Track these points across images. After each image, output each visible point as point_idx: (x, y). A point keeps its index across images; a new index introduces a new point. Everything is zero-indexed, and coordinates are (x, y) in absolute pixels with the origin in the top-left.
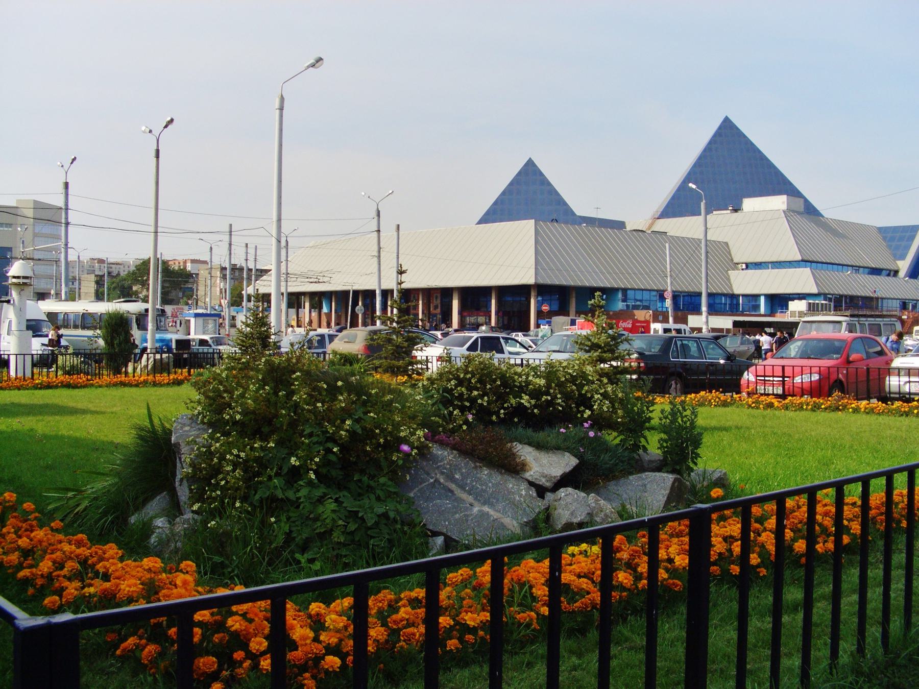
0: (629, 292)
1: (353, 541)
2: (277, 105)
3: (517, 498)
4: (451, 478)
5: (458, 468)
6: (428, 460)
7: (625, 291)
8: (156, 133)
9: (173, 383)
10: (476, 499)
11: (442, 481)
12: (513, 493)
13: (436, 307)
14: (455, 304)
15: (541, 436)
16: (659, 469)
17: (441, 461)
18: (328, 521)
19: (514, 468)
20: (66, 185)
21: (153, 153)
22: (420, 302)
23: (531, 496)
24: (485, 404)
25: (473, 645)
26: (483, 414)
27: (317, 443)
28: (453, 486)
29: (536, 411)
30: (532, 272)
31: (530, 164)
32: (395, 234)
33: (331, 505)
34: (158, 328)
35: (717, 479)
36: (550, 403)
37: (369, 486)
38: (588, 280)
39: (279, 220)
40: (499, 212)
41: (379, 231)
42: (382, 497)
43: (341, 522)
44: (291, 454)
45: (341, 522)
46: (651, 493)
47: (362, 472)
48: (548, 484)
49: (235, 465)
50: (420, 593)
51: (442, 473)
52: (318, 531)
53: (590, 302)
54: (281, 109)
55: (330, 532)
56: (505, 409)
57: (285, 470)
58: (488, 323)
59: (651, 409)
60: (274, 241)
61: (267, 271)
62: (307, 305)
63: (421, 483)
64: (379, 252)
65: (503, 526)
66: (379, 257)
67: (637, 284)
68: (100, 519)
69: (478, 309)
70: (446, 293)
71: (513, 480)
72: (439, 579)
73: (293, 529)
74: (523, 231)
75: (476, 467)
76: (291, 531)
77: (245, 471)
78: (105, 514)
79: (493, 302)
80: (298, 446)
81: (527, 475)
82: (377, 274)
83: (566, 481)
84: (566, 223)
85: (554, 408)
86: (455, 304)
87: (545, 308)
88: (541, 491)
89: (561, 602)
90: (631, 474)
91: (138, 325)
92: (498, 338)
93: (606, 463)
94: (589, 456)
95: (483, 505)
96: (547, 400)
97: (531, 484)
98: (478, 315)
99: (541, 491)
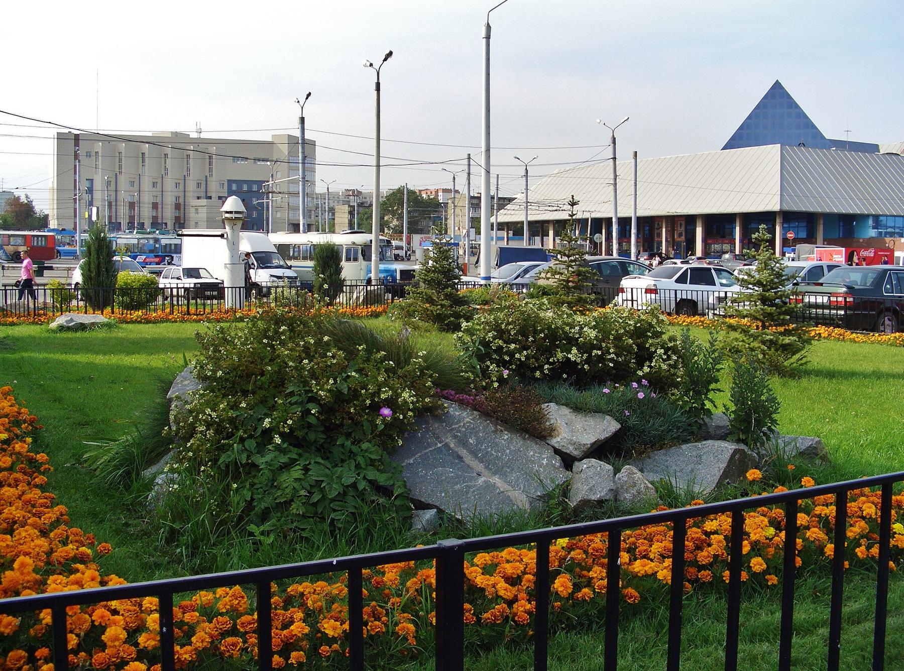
0: (881, 218)
1: (316, 513)
2: (484, 34)
3: (536, 468)
4: (464, 443)
5: (474, 431)
6: (442, 421)
7: (876, 217)
8: (376, 66)
9: (371, 316)
10: (487, 467)
11: (452, 445)
12: (533, 462)
13: (680, 235)
14: (699, 231)
15: (588, 397)
16: (723, 438)
17: (457, 423)
18: (287, 491)
19: (537, 431)
20: (302, 120)
21: (374, 87)
22: (664, 230)
23: (554, 466)
24: (523, 359)
25: (328, 658)
26: (524, 371)
27: (296, 403)
28: (463, 452)
29: (586, 367)
30: (778, 198)
31: (777, 86)
32: (633, 161)
33: (297, 472)
34: (382, 258)
35: (807, 449)
36: (601, 359)
37: (351, 452)
38: (835, 206)
39: (488, 150)
40: (743, 138)
41: (614, 158)
42: (363, 464)
43: (303, 493)
44: (267, 415)
45: (303, 493)
46: (701, 467)
47: (348, 435)
48: (576, 453)
49: (209, 425)
50: (831, 511)
51: (455, 437)
52: (277, 501)
53: (753, 236)
54: (488, 37)
55: (289, 503)
56: (550, 364)
57: (259, 431)
58: (732, 251)
59: (718, 367)
60: (483, 172)
61: (510, 200)
62: (551, 233)
63: (426, 448)
64: (615, 179)
65: (509, 501)
66: (616, 184)
67: (881, 209)
68: (111, 472)
69: (723, 237)
70: (690, 220)
71: (535, 447)
72: (423, 559)
73: (255, 497)
74: (767, 157)
75: (495, 431)
76: (252, 499)
77: (217, 432)
78: (117, 468)
79: (738, 229)
80: (273, 408)
81: (554, 442)
82: (613, 203)
83: (599, 450)
84: (815, 146)
85: (604, 364)
86: (699, 231)
87: (790, 235)
88: (568, 461)
89: (462, 611)
90: (686, 441)
91: (363, 255)
92: (710, 269)
93: (657, 430)
94: (633, 421)
95: (485, 475)
96: (596, 355)
97: (557, 451)
98: (723, 243)
99: (568, 461)
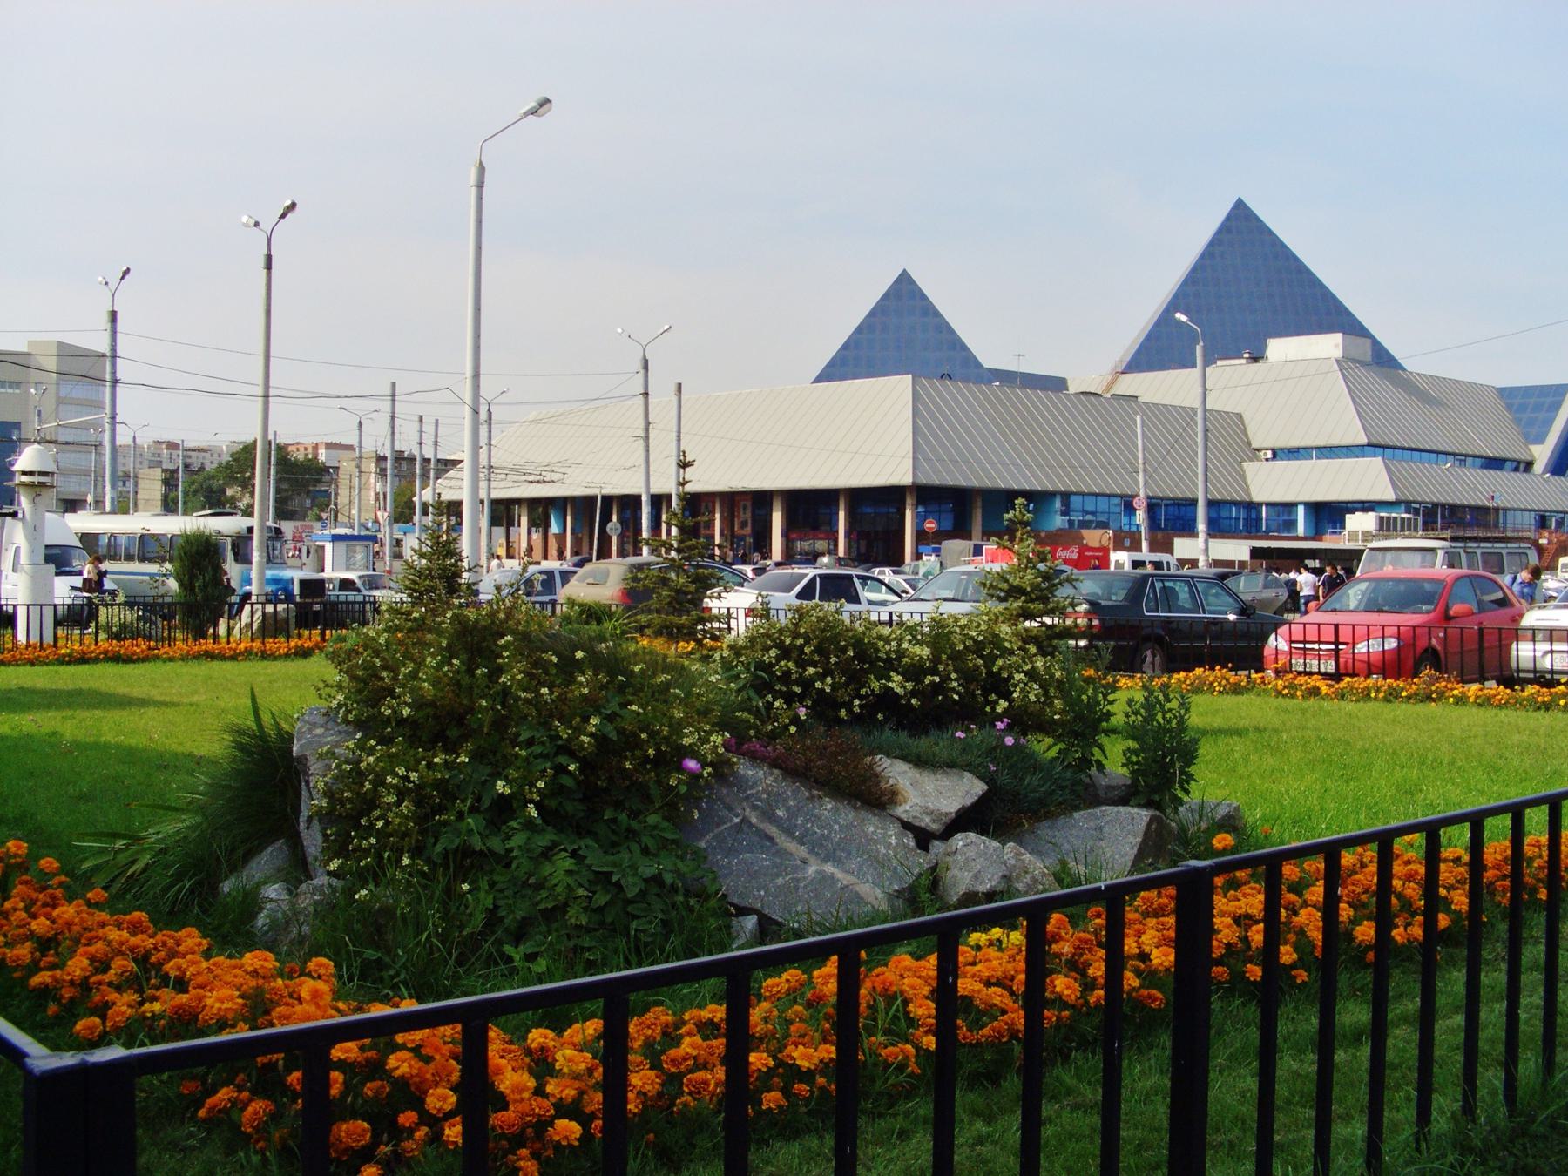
0: (1073, 498)
1: (602, 924)
2: (473, 179)
3: (883, 850)
4: (769, 816)
5: (781, 799)
6: (730, 785)
7: (1066, 496)
8: (266, 226)
9: (296, 654)
10: (811, 851)
11: (754, 820)
12: (876, 842)
13: (744, 524)
14: (777, 519)
15: (923, 744)
16: (1124, 801)
17: (752, 788)
18: (559, 889)
19: (877, 799)
20: (113, 316)
21: (262, 262)
22: (717, 516)
23: (906, 846)
24: (828, 689)
25: (807, 1100)
26: (824, 707)
27: (541, 755)
28: (773, 830)
29: (914, 701)
30: (908, 464)
31: (904, 279)
32: (675, 399)
33: (564, 863)
34: (270, 560)
35: (1223, 818)
36: (938, 688)
37: (629, 830)
38: (1003, 478)
39: (476, 375)
40: (851, 362)
41: (646, 394)
42: (652, 848)
43: (581, 892)
44: (497, 775)
45: (581, 892)
46: (1111, 841)
47: (618, 805)
48: (935, 827)
49: (402, 794)
51: (755, 808)
52: (542, 906)
53: (1006, 516)
54: (480, 186)
55: (563, 908)
56: (861, 698)
57: (486, 802)
58: (833, 551)
59: (1111, 698)
60: (467, 412)
61: (455, 463)
62: (524, 520)
63: (718, 825)
64: (647, 430)
65: (859, 899)
66: (647, 438)
67: (1087, 485)
68: (171, 886)
69: (815, 527)
70: (761, 500)
71: (875, 820)
72: (748, 988)
73: (501, 903)
74: (892, 393)
75: (812, 798)
76: (496, 907)
77: (419, 804)
78: (179, 877)
79: (842, 515)
80: (508, 761)
81: (900, 811)
82: (643, 467)
83: (966, 820)
84: (966, 380)
85: (945, 697)
86: (777, 519)
87: (930, 526)
88: (923, 838)
89: (957, 1027)
90: (1077, 808)
91: (236, 554)
92: (850, 577)
93: (1034, 791)
94: (1005, 779)
95: (823, 863)
96: (933, 683)
97: (907, 826)
98: (815, 538)
99: (923, 838)
